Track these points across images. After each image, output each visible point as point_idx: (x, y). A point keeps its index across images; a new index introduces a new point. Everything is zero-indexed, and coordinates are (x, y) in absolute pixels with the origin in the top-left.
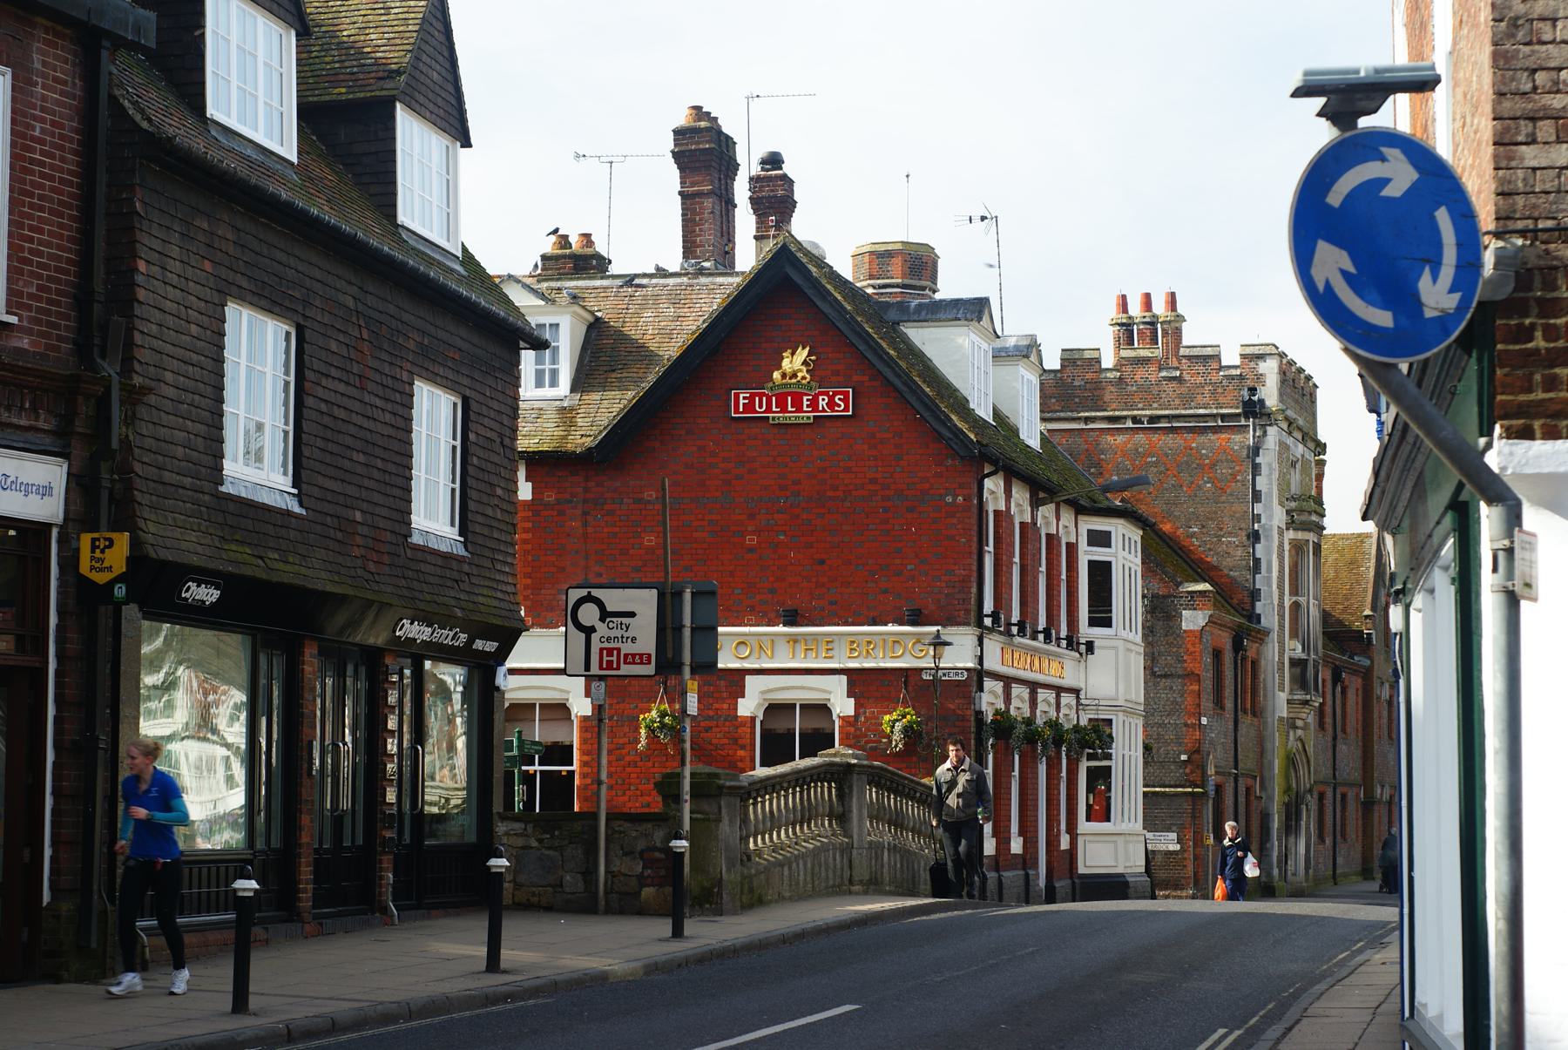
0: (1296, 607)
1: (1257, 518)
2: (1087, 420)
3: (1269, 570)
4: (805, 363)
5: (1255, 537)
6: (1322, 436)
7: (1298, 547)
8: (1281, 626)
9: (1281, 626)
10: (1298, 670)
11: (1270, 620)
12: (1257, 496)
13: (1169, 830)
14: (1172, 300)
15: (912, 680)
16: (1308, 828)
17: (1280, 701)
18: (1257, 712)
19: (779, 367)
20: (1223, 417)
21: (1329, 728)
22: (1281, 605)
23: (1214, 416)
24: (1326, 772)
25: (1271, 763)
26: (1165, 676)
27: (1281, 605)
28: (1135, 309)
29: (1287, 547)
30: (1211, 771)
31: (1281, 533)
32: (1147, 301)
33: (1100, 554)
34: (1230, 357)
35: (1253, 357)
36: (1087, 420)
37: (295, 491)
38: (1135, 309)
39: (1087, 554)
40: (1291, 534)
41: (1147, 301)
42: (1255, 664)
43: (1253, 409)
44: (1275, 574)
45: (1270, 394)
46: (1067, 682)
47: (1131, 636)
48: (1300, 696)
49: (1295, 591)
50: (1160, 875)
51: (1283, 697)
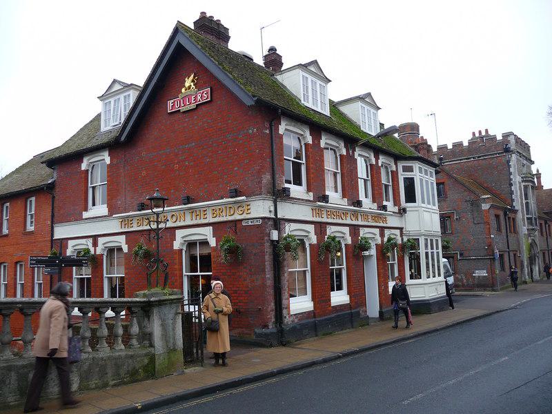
0: (527, 203)
1: (511, 180)
2: (461, 160)
3: (517, 193)
4: (193, 81)
5: (511, 185)
6: (532, 159)
7: (526, 187)
8: (523, 209)
9: (523, 209)
10: (529, 221)
11: (517, 206)
12: (510, 174)
13: (483, 270)
14: (487, 131)
15: (238, 226)
16: (539, 263)
17: (524, 229)
18: (516, 232)
19: (184, 86)
20: (499, 154)
21: (545, 233)
22: (522, 203)
23: (496, 154)
24: (545, 247)
25: (522, 247)
26: (478, 223)
27: (522, 203)
28: (477, 135)
29: (522, 187)
30: (496, 251)
31: (520, 183)
32: (480, 132)
33: (409, 175)
34: (499, 137)
35: (506, 136)
36: (461, 160)
37: (311, 196)
38: (477, 135)
39: (402, 176)
40: (524, 184)
41: (480, 132)
42: (514, 219)
43: (507, 150)
44: (519, 194)
45: (512, 146)
46: (477, 226)
47: (434, 207)
48: (531, 227)
49: (526, 198)
50: (449, 301)
51: (525, 228)
